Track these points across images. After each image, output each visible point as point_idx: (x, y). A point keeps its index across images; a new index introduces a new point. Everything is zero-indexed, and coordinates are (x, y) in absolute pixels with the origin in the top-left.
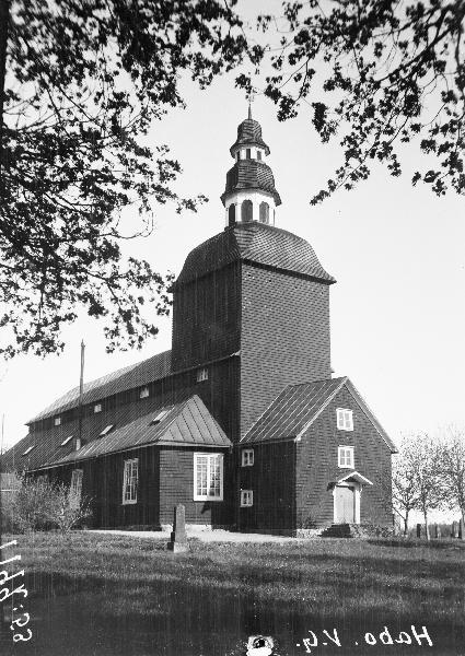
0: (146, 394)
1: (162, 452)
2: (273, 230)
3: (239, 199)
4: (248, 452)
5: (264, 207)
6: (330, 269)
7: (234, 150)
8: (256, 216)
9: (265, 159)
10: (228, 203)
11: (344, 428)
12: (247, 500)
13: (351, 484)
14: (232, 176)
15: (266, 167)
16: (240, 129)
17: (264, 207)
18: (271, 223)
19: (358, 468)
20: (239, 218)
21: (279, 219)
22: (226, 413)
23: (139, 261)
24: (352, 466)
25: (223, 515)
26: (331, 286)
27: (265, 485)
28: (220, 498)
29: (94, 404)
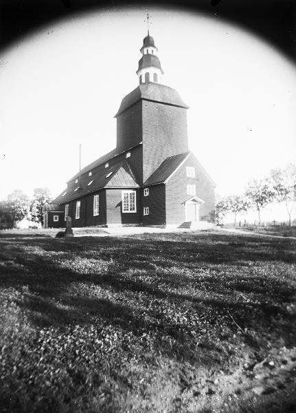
0: (107, 166)
1: (107, 191)
2: (159, 85)
3: (144, 72)
4: (146, 189)
5: (155, 75)
6: (185, 101)
7: (142, 50)
8: (151, 79)
9: (155, 54)
10: (140, 74)
11: (191, 176)
12: (146, 212)
13: (194, 203)
14: (141, 62)
15: (155, 57)
16: (144, 40)
17: (155, 75)
18: (159, 82)
19: (197, 195)
20: (143, 81)
21: (161, 80)
22: (138, 176)
23: (141, 56)
24: (195, 194)
25: (127, 219)
26: (188, 110)
27: (151, 202)
28: (135, 211)
29: (105, 163)
